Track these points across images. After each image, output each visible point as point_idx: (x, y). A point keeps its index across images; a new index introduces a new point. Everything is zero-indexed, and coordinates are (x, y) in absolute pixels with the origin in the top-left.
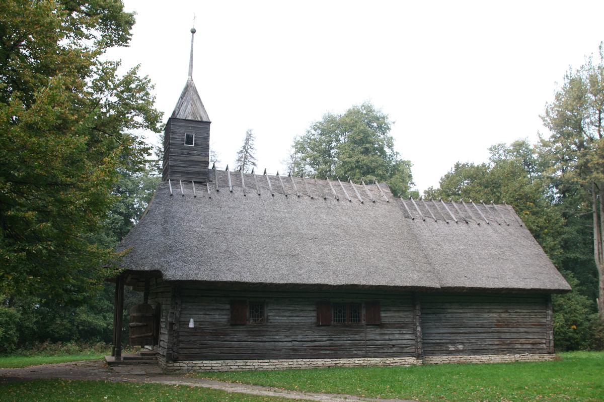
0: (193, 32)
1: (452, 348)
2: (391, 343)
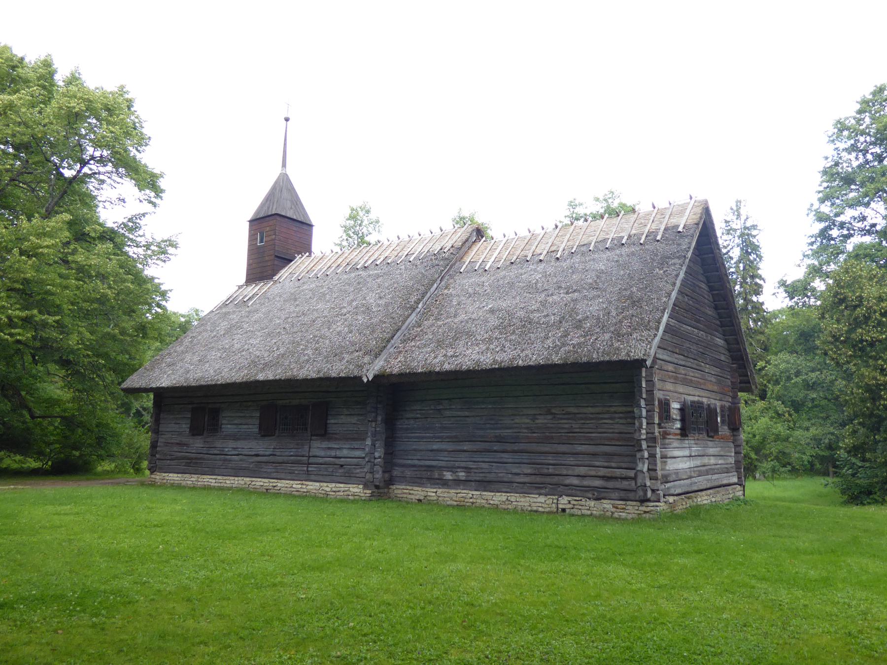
0: (287, 120)
1: (448, 476)
2: (338, 463)
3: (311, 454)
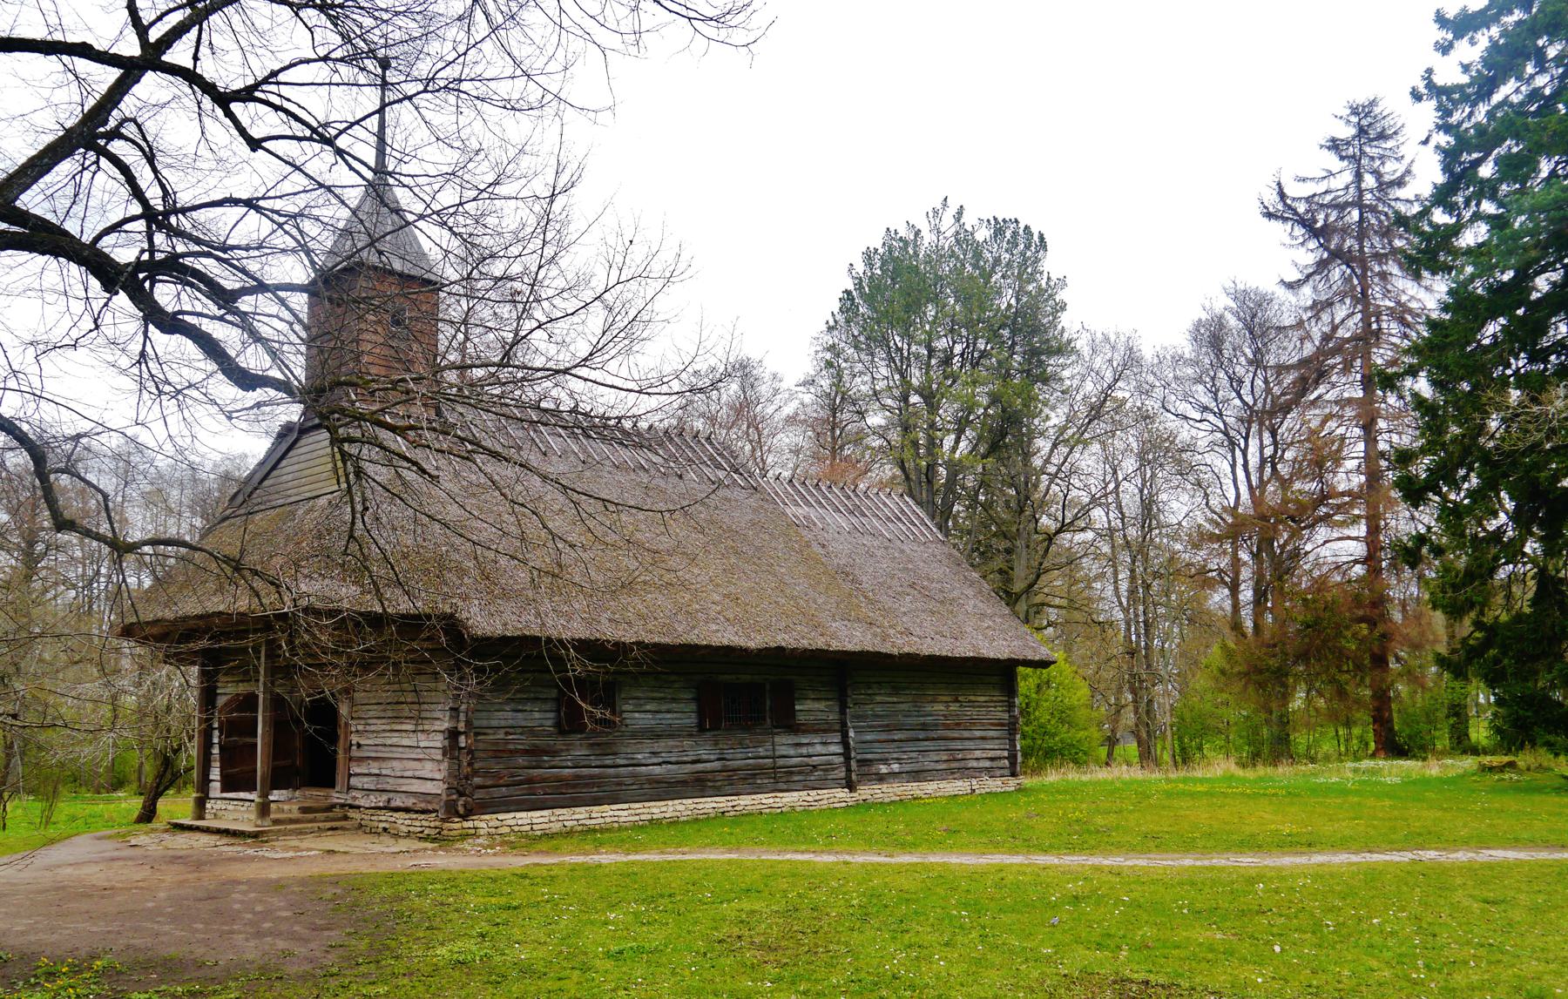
1: (884, 769)
3: (777, 753)
